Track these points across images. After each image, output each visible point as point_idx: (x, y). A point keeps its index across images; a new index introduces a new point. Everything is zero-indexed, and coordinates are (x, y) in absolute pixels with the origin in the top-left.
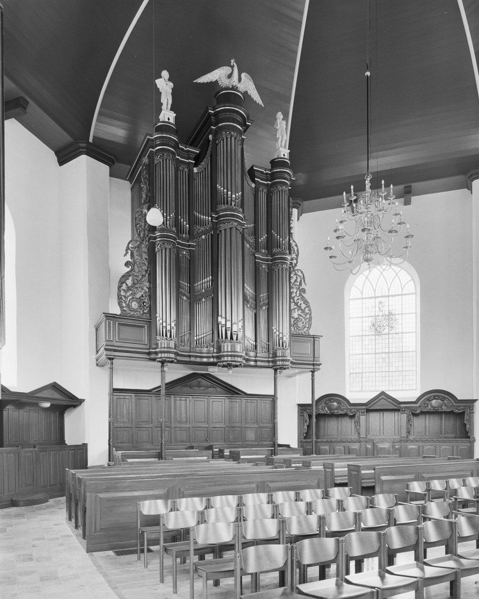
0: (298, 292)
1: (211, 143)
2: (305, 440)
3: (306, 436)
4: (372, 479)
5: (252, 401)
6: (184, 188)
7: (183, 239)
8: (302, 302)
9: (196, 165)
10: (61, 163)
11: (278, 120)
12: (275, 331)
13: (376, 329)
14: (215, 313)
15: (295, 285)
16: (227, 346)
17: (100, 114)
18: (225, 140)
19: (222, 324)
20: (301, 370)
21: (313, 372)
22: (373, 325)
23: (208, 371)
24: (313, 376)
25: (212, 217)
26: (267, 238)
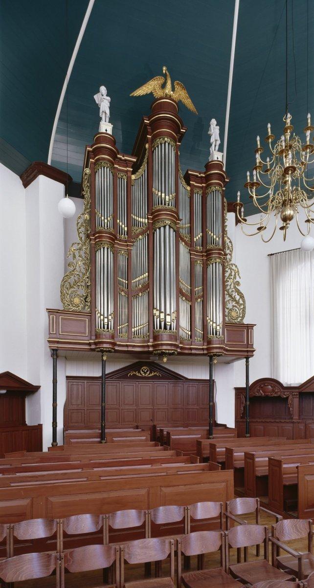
0: (233, 285)
1: (147, 151)
2: (242, 420)
3: (241, 414)
4: (295, 473)
5: (194, 385)
6: (122, 194)
8: (236, 294)
9: (134, 173)
10: (26, 184)
11: (212, 126)
12: (209, 321)
14: (151, 306)
15: (230, 279)
17: (55, 141)
18: (160, 146)
20: (238, 357)
21: (247, 358)
23: (150, 359)
24: (247, 362)
25: (148, 218)
26: (202, 237)
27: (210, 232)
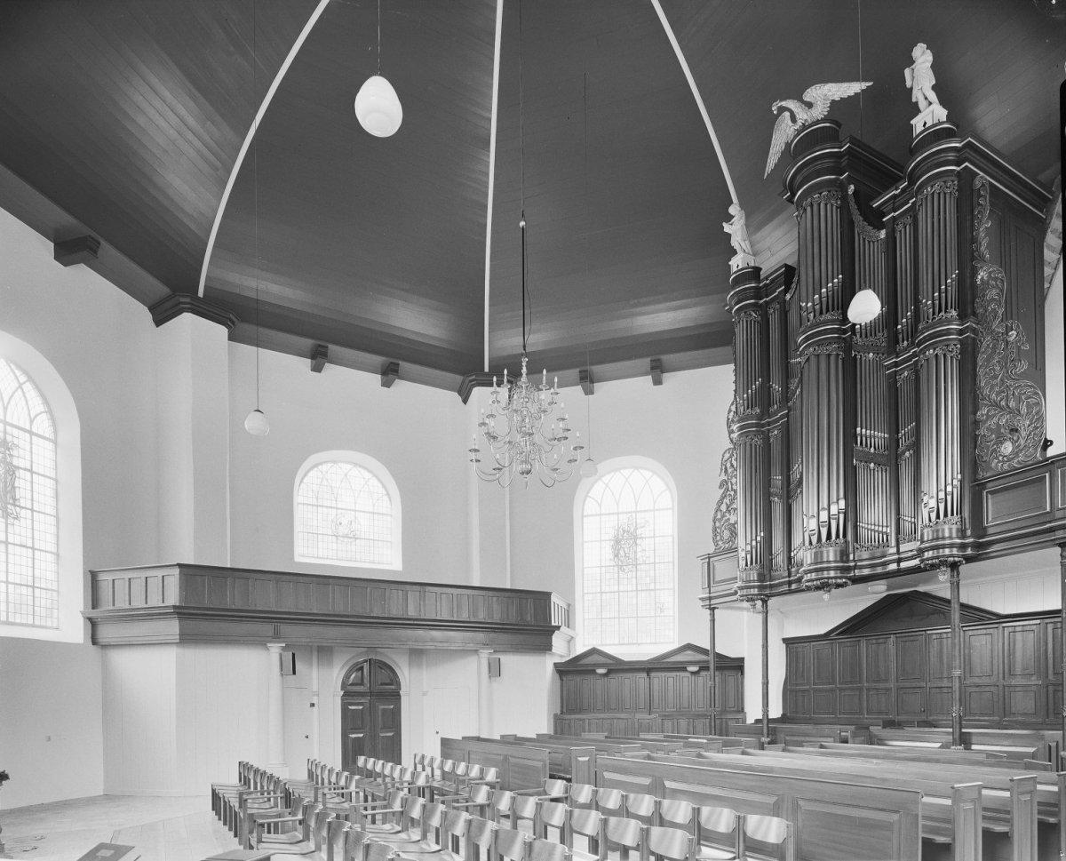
7: (906, 350)
10: (159, 322)
16: (828, 552)
24: (713, 615)
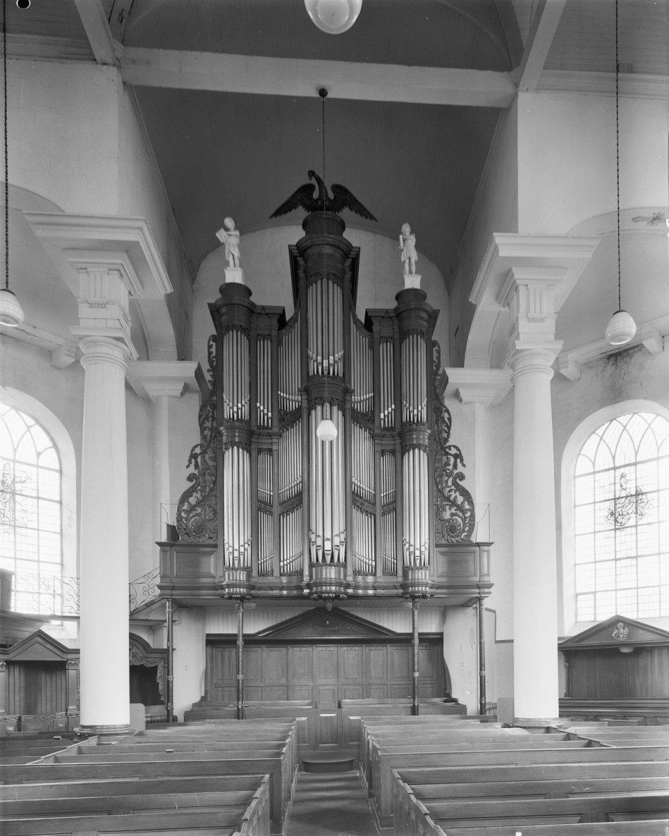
8: (458, 493)
13: (616, 521)
14: (307, 527)
19: (318, 544)
22: (612, 514)
27: (405, 402)
